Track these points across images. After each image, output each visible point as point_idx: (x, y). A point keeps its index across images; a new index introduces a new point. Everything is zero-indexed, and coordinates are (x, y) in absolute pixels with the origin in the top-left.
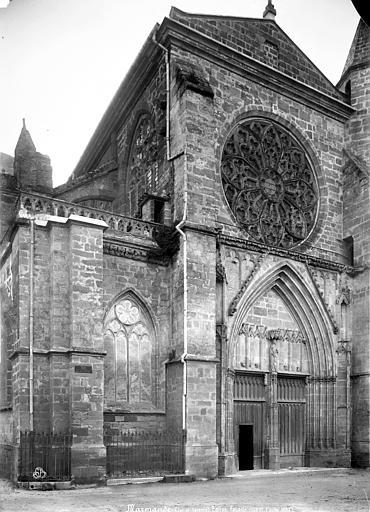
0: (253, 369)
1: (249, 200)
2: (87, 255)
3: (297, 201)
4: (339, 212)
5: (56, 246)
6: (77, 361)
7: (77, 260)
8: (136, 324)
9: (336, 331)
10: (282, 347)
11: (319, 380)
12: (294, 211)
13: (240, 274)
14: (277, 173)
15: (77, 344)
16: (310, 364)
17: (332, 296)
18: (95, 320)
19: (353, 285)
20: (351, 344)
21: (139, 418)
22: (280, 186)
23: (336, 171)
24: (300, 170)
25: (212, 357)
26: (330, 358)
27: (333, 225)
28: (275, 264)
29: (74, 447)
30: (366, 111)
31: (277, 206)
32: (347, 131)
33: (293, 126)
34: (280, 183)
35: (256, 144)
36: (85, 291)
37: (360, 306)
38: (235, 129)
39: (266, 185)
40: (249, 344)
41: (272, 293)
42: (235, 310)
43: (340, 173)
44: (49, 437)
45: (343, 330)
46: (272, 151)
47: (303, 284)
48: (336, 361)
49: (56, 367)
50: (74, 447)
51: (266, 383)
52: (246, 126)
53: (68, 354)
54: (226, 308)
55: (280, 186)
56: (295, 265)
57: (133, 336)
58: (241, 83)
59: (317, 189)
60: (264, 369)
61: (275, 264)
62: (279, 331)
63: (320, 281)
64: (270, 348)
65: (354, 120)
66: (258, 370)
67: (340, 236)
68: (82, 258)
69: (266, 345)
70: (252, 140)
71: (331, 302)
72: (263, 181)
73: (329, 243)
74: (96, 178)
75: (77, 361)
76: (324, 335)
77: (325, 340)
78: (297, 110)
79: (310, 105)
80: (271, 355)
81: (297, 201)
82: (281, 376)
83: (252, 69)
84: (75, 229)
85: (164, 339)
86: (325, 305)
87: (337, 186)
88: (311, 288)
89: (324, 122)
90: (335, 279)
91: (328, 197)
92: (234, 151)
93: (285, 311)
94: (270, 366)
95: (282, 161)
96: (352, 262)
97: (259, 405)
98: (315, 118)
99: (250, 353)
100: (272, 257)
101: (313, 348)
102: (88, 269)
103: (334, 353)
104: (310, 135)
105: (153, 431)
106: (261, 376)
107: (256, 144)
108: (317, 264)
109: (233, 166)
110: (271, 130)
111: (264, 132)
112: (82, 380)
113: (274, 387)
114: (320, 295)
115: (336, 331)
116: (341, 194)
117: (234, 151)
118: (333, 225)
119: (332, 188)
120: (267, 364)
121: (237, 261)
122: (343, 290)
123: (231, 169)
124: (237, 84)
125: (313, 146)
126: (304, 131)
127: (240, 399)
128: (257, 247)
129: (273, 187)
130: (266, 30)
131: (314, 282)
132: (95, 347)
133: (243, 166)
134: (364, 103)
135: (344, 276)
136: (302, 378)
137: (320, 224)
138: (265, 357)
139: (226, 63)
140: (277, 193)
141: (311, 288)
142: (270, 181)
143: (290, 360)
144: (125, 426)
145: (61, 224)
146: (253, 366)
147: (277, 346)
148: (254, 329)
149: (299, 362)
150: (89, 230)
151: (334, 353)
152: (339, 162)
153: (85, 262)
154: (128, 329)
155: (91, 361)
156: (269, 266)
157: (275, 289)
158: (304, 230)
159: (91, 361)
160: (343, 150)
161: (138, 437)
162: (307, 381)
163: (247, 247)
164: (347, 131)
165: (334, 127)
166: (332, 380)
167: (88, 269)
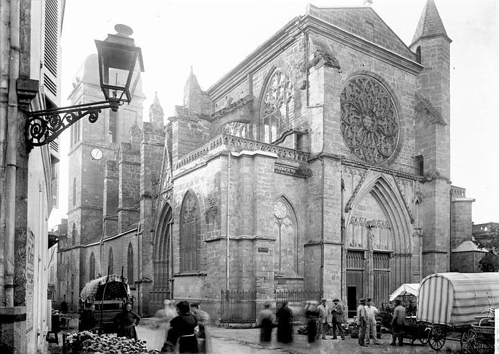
0: (357, 248)
1: (355, 131)
2: (265, 176)
3: (386, 130)
4: (412, 137)
5: (246, 170)
6: (259, 244)
7: (260, 179)
8: (285, 218)
9: (412, 221)
10: (376, 232)
11: (400, 255)
12: (383, 137)
13: (353, 184)
14: (373, 112)
15: (259, 234)
16: (394, 244)
17: (410, 196)
18: (270, 218)
19: (425, 188)
20: (422, 231)
21: (288, 282)
22: (374, 121)
23: (411, 109)
24: (387, 109)
25: (338, 241)
26: (408, 241)
27: (409, 147)
28: (374, 176)
29: (257, 300)
30: (431, 69)
31: (372, 134)
32: (418, 80)
33: (384, 80)
34: (374, 118)
35: (359, 93)
36: (264, 199)
37: (429, 204)
38: (346, 85)
39: (365, 120)
40: (355, 230)
41: (370, 195)
42: (350, 209)
43: (413, 110)
44: (240, 296)
45: (417, 220)
46: (369, 97)
47: (391, 189)
48: (412, 243)
49: (245, 248)
50: (257, 300)
51: (365, 257)
52: (354, 81)
53: (253, 240)
54: (344, 206)
55: (374, 121)
56: (388, 177)
57: (283, 226)
58: (351, 53)
59: (397, 122)
60: (364, 247)
61: (374, 176)
62: (374, 221)
63: (402, 187)
64: (369, 233)
65: (422, 74)
66: (361, 248)
67: (413, 154)
68: (263, 178)
69: (366, 231)
70: (357, 90)
71: (409, 201)
72: (364, 117)
73: (407, 159)
74: (239, 108)
75: (259, 244)
76: (404, 224)
77: (405, 228)
78: (386, 69)
79: (395, 64)
80: (369, 238)
81: (386, 130)
82: (375, 253)
83: (358, 44)
84: (258, 159)
85: (303, 228)
86: (405, 204)
87: (411, 119)
88: (396, 192)
89: (403, 75)
90: (411, 185)
91: (405, 128)
92: (346, 98)
93: (377, 207)
94: (368, 245)
95: (376, 103)
96: (421, 173)
97: (360, 272)
98: (397, 73)
99: (357, 238)
100: (372, 171)
101: (396, 232)
102: (266, 185)
103: (411, 236)
104: (393, 84)
105: (295, 291)
106: (362, 252)
107: (359, 93)
108: (400, 175)
109: (345, 108)
110: (369, 82)
111: (365, 85)
112: (259, 257)
113: (371, 261)
114: (402, 196)
115: (412, 221)
116: (414, 124)
117: (346, 98)
118: (409, 147)
119: (409, 121)
120: (366, 244)
121: (350, 175)
122: (417, 193)
123: (344, 111)
124: (349, 53)
125: (396, 93)
126: (390, 82)
127: (353, 268)
128: (363, 166)
129: (371, 122)
130: (373, 20)
131: (398, 188)
132: (269, 236)
133: (351, 108)
134: (430, 63)
135: (417, 183)
136: (388, 254)
137: (400, 145)
138: (365, 239)
139: (343, 41)
140: (372, 125)
141: (396, 192)
142: (368, 117)
143: (381, 242)
144: (279, 287)
145: (249, 156)
146: (357, 246)
147: (373, 231)
148: (358, 220)
149: (386, 243)
150: (267, 159)
151: (411, 236)
152: (413, 102)
153: (264, 180)
154: (280, 221)
155: (266, 244)
156: (371, 177)
157: (372, 193)
158: (389, 150)
159: (266, 244)
160: (416, 95)
161: (233, 295)
162: (391, 256)
163: (358, 166)
164: (418, 80)
165: (410, 79)
166: (410, 255)
167: (266, 185)
